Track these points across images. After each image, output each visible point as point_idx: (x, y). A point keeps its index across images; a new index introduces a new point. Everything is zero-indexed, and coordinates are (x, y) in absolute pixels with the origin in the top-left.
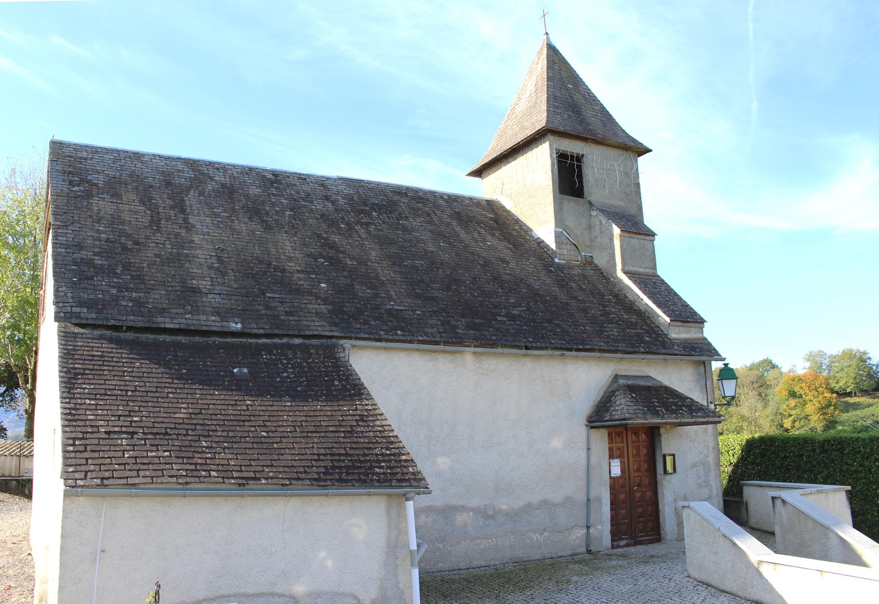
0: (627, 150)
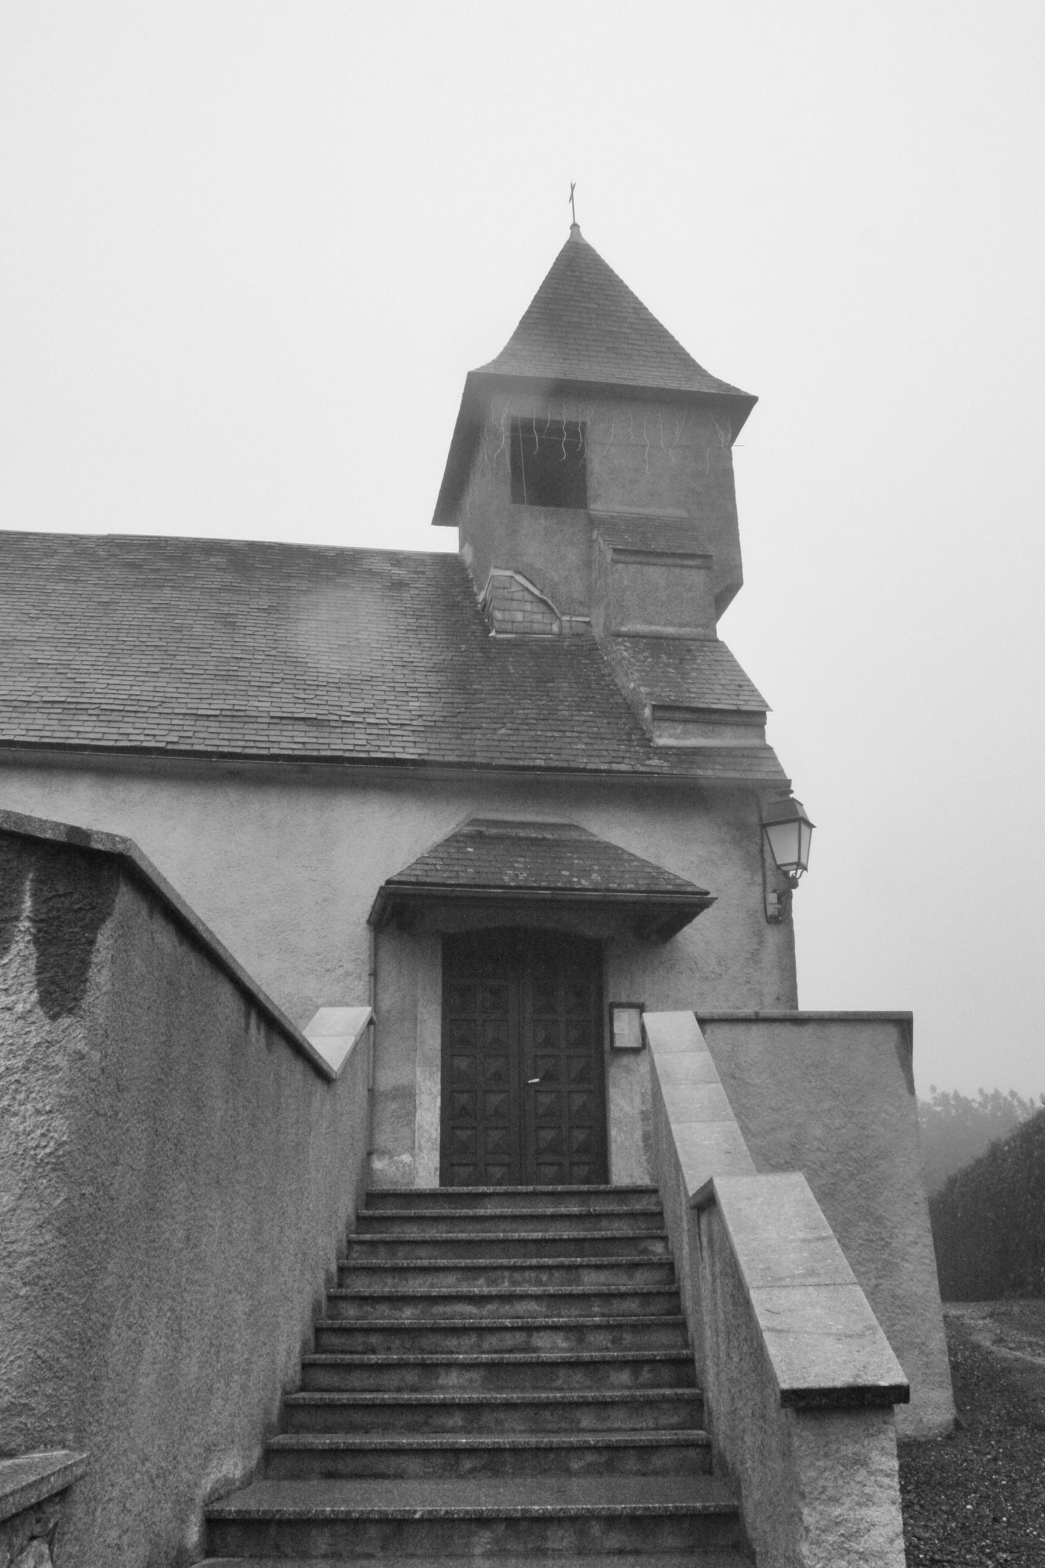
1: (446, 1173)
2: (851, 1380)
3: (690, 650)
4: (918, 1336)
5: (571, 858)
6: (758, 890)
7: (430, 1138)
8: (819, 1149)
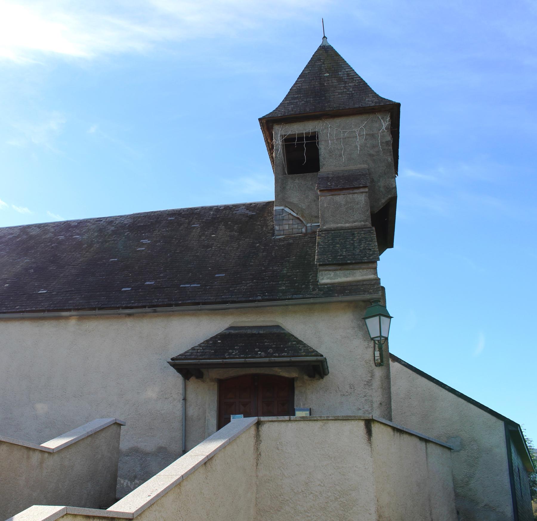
6: (371, 350)
8: (319, 485)
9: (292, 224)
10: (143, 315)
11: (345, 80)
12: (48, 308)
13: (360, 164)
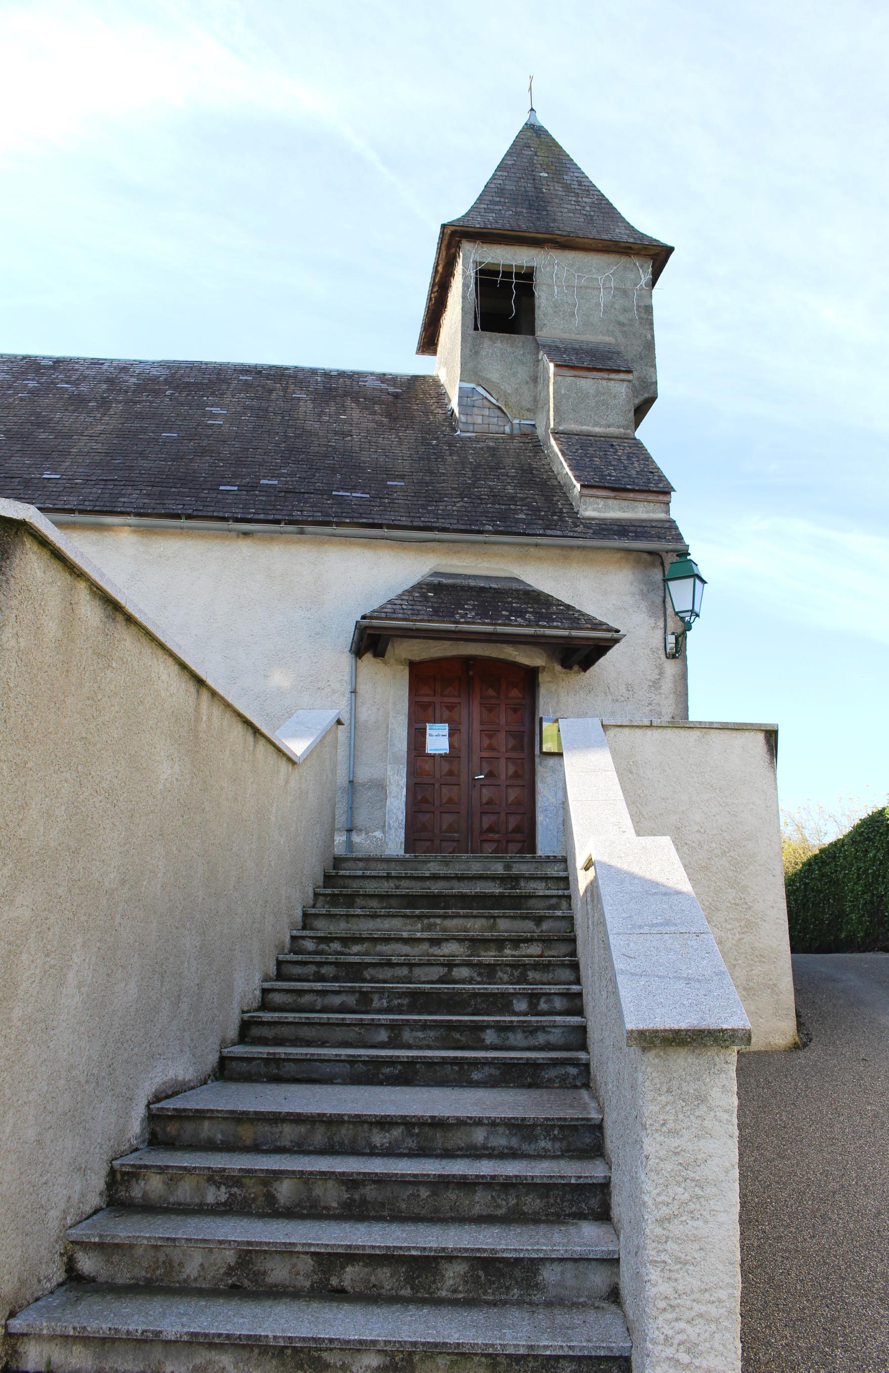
0: (628, 254)
1: (410, 845)
2: (695, 1022)
3: (613, 445)
4: (771, 979)
5: (511, 603)
7: (397, 819)
8: (698, 831)
9: (489, 416)
10: (271, 537)
11: (577, 191)
12: (81, 507)
13: (603, 335)
